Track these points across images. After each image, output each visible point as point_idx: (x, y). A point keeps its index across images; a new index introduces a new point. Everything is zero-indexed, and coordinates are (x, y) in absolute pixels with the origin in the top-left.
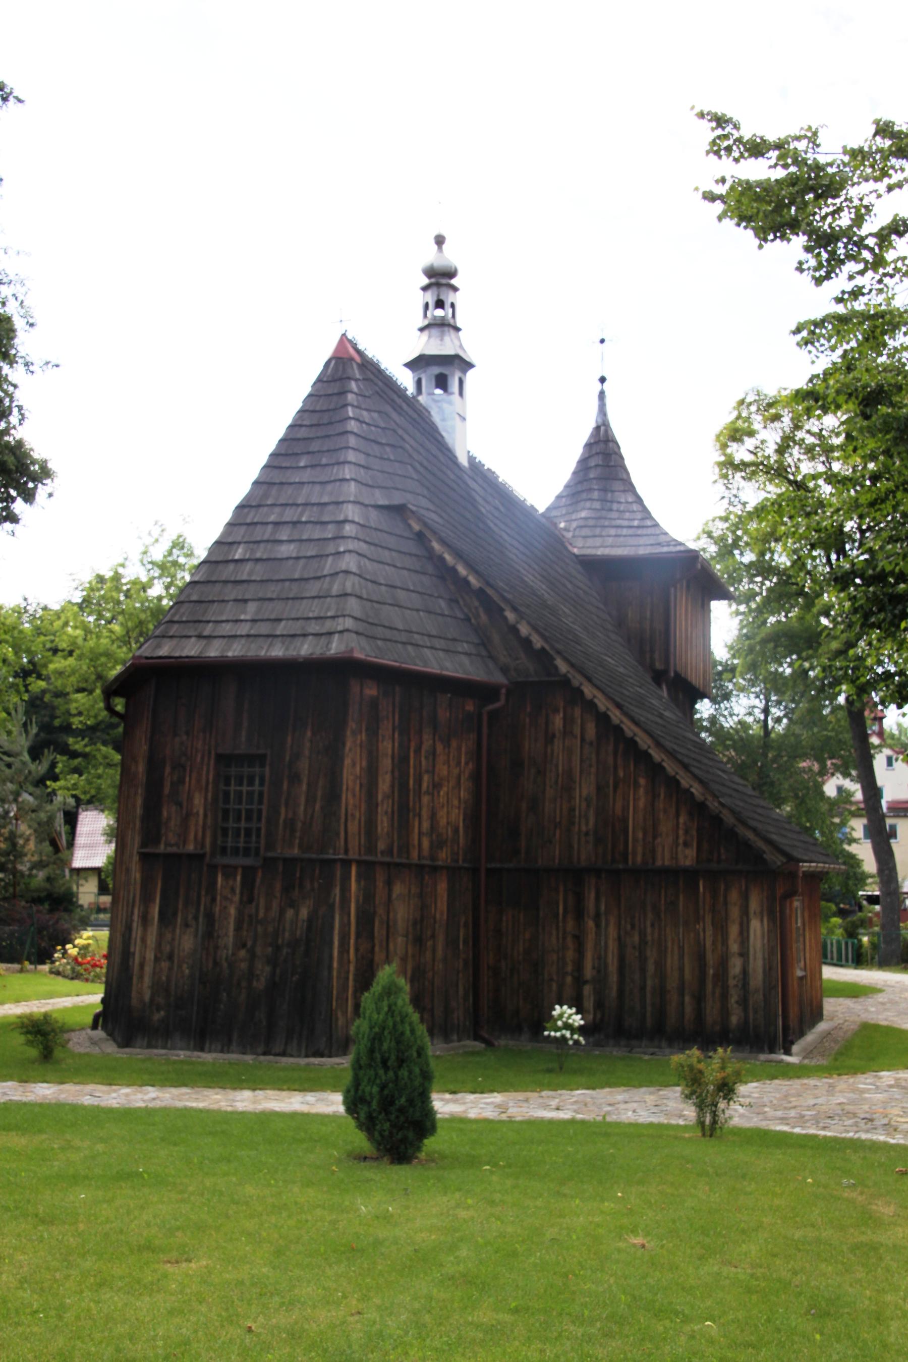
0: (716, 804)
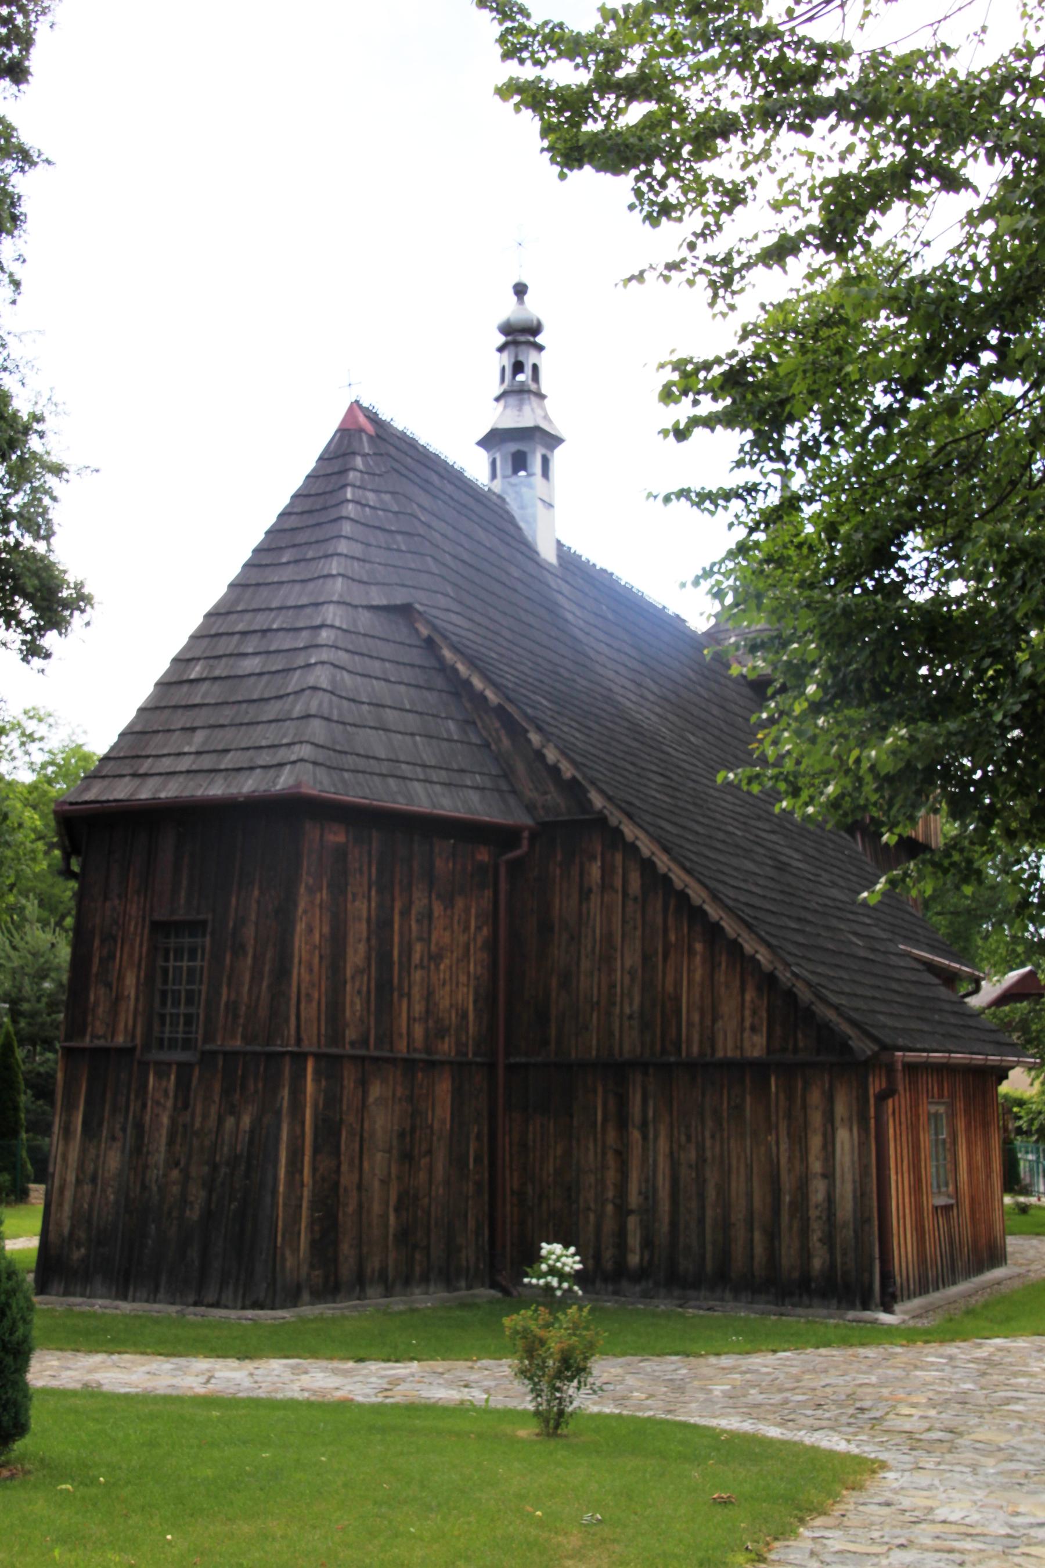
0: (788, 975)
